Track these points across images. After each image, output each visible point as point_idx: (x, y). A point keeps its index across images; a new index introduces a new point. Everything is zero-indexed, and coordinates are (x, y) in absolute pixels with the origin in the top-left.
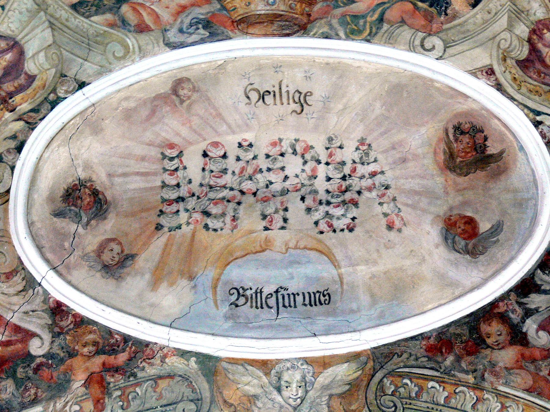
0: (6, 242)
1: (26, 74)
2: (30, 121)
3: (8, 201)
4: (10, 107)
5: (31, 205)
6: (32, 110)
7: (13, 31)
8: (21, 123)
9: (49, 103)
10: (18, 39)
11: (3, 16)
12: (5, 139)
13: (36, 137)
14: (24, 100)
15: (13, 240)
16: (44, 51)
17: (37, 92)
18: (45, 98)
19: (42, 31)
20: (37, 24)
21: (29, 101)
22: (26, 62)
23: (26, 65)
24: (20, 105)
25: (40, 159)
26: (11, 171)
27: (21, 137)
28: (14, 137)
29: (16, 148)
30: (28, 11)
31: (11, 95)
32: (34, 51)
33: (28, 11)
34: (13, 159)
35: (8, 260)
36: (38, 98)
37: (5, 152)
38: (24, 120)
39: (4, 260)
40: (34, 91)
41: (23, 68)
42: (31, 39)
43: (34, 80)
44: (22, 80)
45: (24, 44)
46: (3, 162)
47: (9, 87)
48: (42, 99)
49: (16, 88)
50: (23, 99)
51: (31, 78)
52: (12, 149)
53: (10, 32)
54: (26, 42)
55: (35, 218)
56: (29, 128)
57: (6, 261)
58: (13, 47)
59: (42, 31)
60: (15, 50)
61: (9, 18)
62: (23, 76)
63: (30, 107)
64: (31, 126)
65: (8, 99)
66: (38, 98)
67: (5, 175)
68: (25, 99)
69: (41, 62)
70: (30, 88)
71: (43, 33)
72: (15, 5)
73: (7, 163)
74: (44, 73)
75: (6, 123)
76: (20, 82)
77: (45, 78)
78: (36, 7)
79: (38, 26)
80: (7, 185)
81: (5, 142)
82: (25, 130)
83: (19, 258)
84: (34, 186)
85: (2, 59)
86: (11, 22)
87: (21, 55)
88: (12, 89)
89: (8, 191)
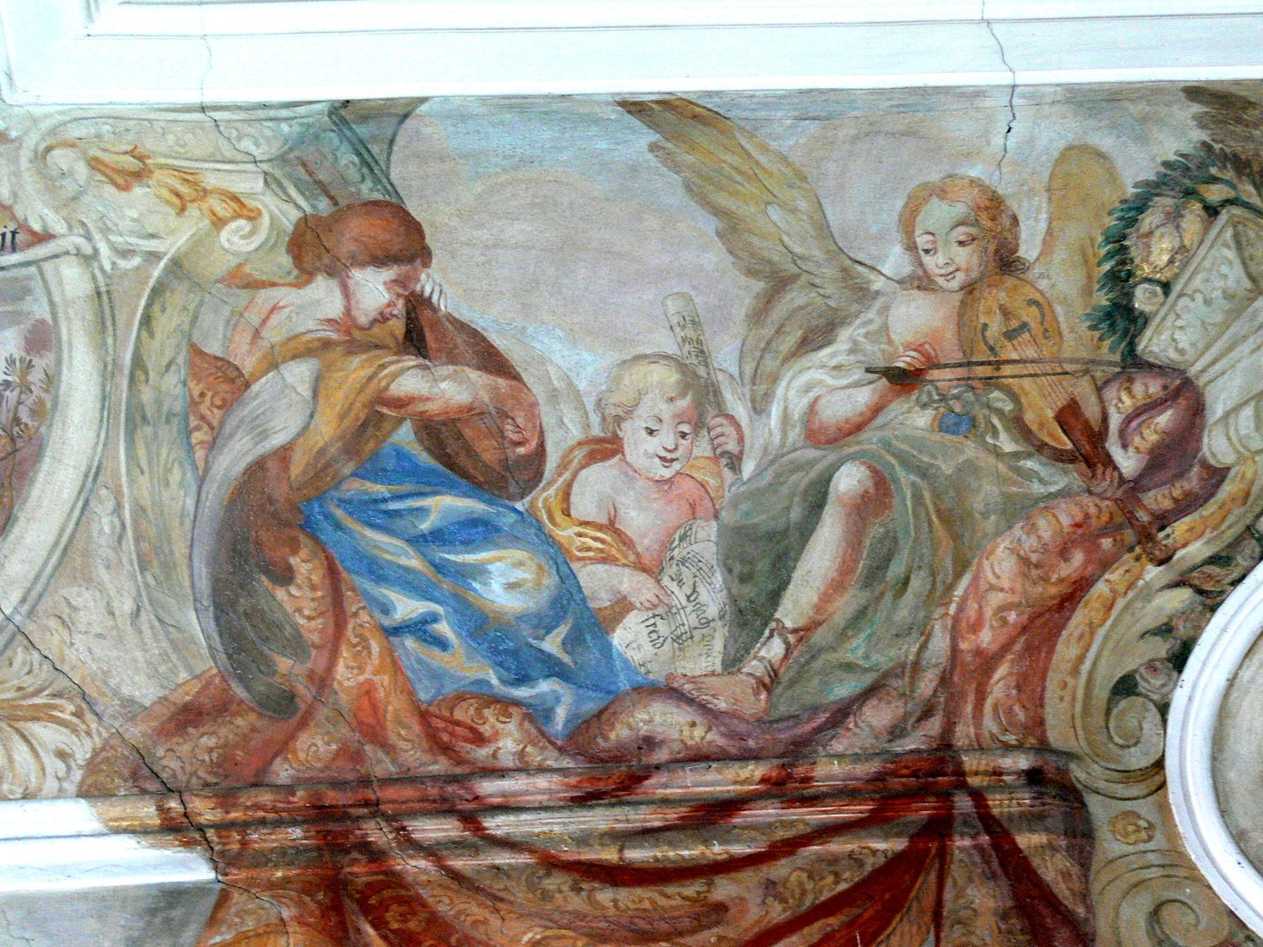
0: (1186, 878)
1: (1205, 465)
2: (1207, 587)
3: (1163, 785)
4: (1157, 553)
5: (1226, 796)
6: (1213, 560)
7: (1182, 352)
8: (1185, 594)
9: (1258, 540)
10: (1192, 371)
11: (1165, 309)
12: (1142, 636)
13: (1222, 625)
14: (1194, 534)
15: (1203, 872)
16: (1253, 403)
17: (1229, 511)
18: (1248, 528)
19: (1253, 351)
20: (1243, 333)
21: (1208, 535)
22: (1206, 432)
23: (1205, 440)
24: (1185, 545)
25: (1232, 682)
26: (1159, 717)
27: (1182, 630)
28: (1165, 630)
29: (1169, 660)
30: (1228, 296)
31: (1163, 520)
32: (1230, 405)
33: (1228, 296)
34: (1163, 685)
35: (1204, 921)
36: (1230, 527)
37: (1142, 670)
38: (1191, 586)
39: (1191, 918)
40: (1220, 508)
41: (1198, 449)
42: (1223, 373)
43: (1221, 481)
44: (1193, 480)
45: (1206, 385)
46: (1138, 695)
47: (1160, 498)
48: (1239, 528)
49: (1176, 501)
50: (1191, 529)
51: (1217, 475)
52: (1161, 660)
53: (1173, 355)
54: (1210, 382)
55: (1245, 823)
56: (1204, 605)
57: (1198, 922)
58: (1177, 393)
59: (1253, 351)
60: (1182, 402)
61: (1178, 316)
62: (1196, 469)
63: (1208, 552)
64: (1208, 602)
65: (1154, 531)
66: (1230, 527)
67: (1146, 726)
68: (1199, 529)
69: (1243, 432)
70: (1212, 501)
71: (1255, 356)
72: (1197, 282)
73: (1147, 697)
74: (1250, 462)
75: (1148, 594)
76: (1187, 486)
77: (1249, 475)
78: (1247, 284)
79: (1245, 338)
80: (1152, 751)
81: (1141, 642)
82: (1193, 611)
83: (1231, 914)
84: (1221, 751)
85: (1149, 427)
86: (1181, 328)
87: (1195, 415)
88: (1167, 504)
89: (1159, 764)
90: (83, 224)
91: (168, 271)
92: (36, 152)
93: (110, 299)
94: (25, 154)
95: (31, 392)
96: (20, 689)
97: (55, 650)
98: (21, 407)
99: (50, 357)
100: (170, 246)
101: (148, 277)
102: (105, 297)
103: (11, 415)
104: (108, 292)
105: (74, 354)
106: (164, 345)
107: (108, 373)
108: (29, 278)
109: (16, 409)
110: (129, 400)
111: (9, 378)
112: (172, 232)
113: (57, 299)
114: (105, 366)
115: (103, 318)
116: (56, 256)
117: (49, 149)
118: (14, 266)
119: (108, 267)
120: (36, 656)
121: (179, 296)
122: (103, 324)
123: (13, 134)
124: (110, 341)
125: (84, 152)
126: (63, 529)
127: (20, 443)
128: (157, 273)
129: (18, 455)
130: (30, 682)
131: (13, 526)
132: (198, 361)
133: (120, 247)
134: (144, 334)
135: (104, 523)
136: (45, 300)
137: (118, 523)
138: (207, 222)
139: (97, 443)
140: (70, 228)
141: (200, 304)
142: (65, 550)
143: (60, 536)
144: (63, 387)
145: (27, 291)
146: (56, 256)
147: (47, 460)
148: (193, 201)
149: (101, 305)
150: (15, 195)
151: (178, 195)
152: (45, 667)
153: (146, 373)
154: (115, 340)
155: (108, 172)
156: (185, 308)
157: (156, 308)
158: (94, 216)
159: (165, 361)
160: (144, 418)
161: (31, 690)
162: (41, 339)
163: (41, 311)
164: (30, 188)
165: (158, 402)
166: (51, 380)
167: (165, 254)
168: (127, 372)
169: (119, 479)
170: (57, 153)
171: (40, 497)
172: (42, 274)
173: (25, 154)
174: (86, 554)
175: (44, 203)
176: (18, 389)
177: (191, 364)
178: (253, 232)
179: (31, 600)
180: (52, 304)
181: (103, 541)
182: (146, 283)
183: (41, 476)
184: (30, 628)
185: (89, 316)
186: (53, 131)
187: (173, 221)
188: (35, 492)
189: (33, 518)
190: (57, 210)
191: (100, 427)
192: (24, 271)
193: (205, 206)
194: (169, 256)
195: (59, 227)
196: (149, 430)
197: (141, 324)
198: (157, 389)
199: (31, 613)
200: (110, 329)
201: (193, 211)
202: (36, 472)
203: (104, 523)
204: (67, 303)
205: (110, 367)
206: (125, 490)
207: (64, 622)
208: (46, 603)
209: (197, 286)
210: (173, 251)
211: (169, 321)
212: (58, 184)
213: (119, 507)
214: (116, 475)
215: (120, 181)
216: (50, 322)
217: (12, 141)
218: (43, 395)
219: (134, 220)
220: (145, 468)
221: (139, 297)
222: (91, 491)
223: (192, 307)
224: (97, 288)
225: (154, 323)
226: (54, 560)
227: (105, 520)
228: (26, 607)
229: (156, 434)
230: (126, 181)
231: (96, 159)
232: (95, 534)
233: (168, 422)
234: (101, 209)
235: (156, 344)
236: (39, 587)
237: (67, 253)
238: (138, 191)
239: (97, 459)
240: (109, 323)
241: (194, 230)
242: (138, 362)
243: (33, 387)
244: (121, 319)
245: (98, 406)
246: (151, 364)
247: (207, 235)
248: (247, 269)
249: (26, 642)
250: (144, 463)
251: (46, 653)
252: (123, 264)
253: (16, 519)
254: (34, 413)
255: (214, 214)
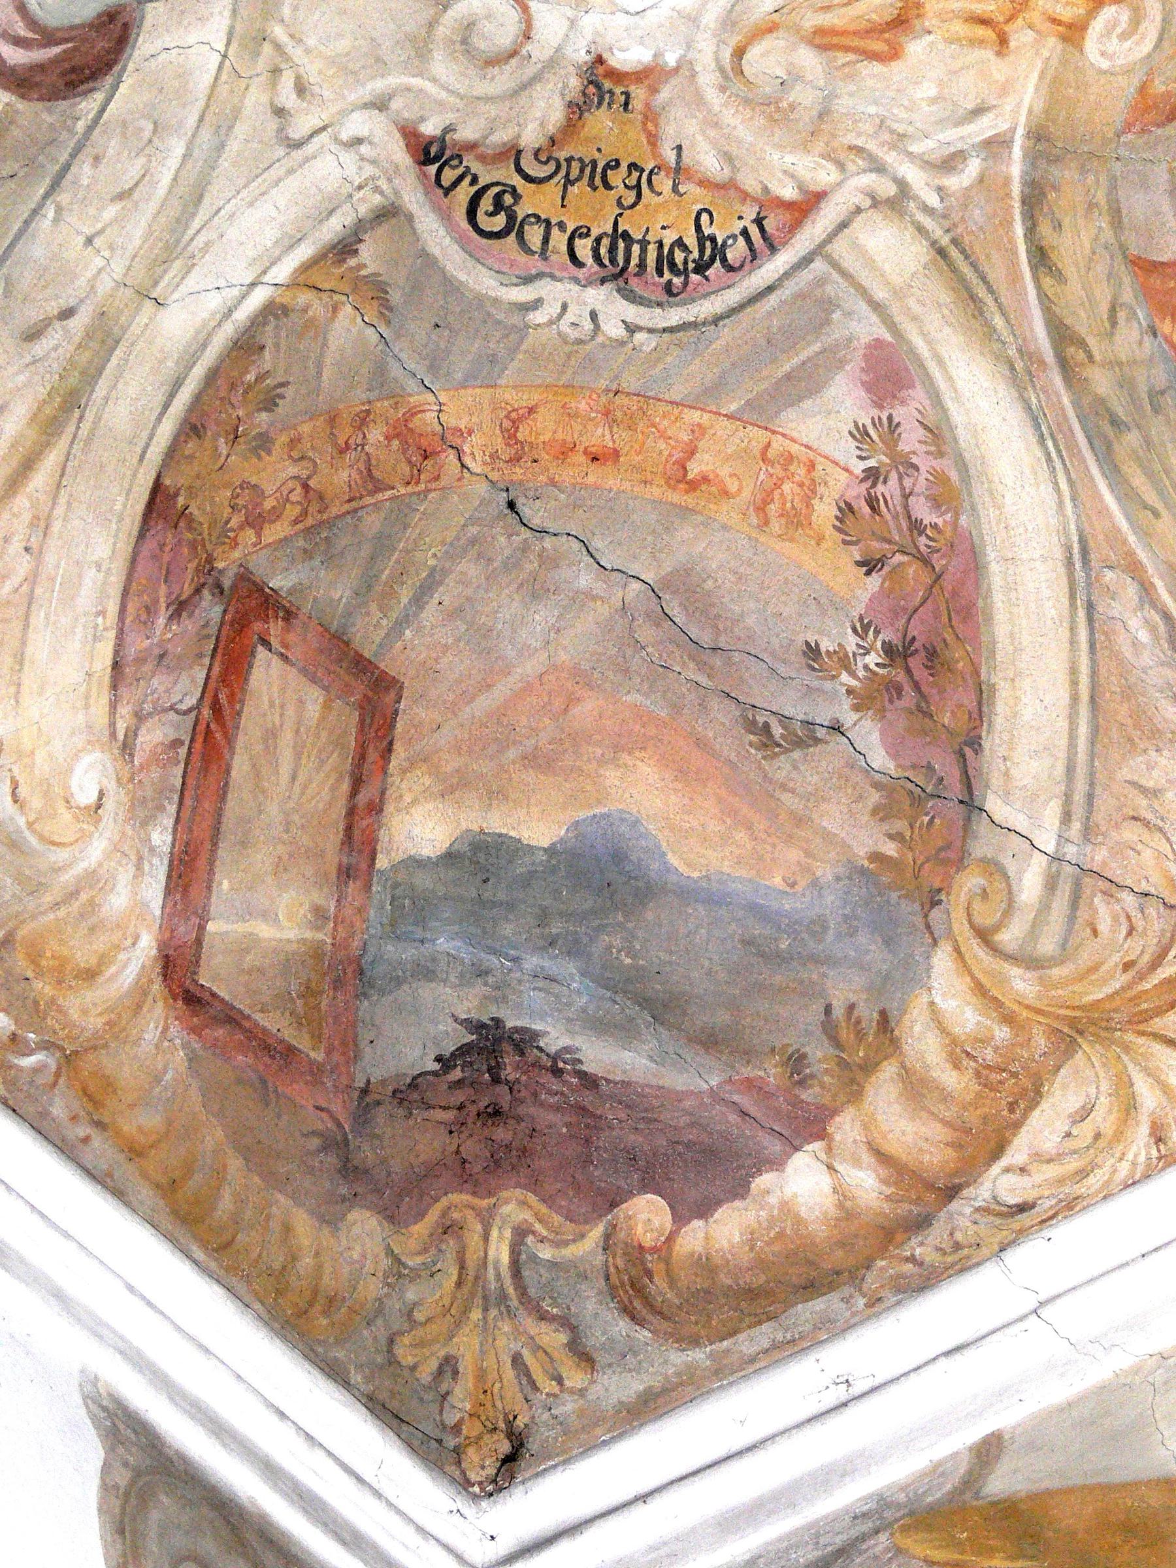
24: (148, 295)
90: (858, 150)
91: (1033, 158)
92: (722, 70)
93: (963, 252)
94: (707, 79)
95: (917, 468)
96: (1127, 966)
97: (1156, 878)
98: (912, 500)
99: (918, 396)
100: (1016, 112)
101: (1007, 181)
102: (954, 253)
103: (904, 525)
104: (955, 242)
105: (953, 372)
106: (1090, 281)
107: (1020, 373)
108: (821, 282)
109: (906, 507)
110: (1076, 405)
111: (872, 463)
112: (1004, 90)
113: (880, 294)
114: (1012, 368)
115: (968, 288)
116: (843, 225)
117: (739, 53)
118: (787, 275)
119: (933, 200)
120: (1129, 899)
121: (1072, 186)
122: (973, 297)
123: (671, 59)
124: (998, 321)
125: (797, 29)
126: (1073, 671)
127: (939, 563)
128: (1016, 168)
129: (947, 583)
130: (1141, 948)
131: (992, 704)
132: (1156, 281)
133: (934, 157)
134: (1047, 282)
135: (1136, 630)
136: (863, 306)
137: (1157, 618)
138: (1052, 41)
139: (1061, 504)
140: (841, 166)
141: (1113, 187)
142: (1093, 699)
143: (1074, 683)
144: (961, 433)
145: (829, 305)
146: (843, 225)
147: (994, 567)
148: (1011, 19)
149: (954, 270)
150: (728, 158)
151: (984, 22)
152: (1152, 912)
153: (1082, 344)
154: (1004, 314)
155: (856, 42)
156: (1091, 206)
157: (1045, 229)
158: (868, 127)
159: (1104, 308)
160: (1115, 422)
161: (1146, 958)
162: (890, 373)
163: (866, 328)
164: (744, 133)
165: (1126, 384)
166: (938, 435)
167: (1013, 130)
168: (1049, 356)
169: (1125, 542)
170: (753, 53)
171: (1012, 634)
172: (835, 265)
173: (707, 79)
174: (1128, 693)
175: (780, 147)
176: (894, 476)
177: (1147, 293)
178: (1137, 19)
179: (1078, 812)
180: (876, 306)
181: (1146, 659)
182: (1008, 195)
183: (998, 599)
184: (1099, 857)
185: (945, 297)
186: (729, 22)
187: (999, 69)
188: (1001, 629)
189: (1019, 674)
190: (805, 147)
191: (1053, 471)
192: (806, 276)
193: (1035, 16)
194: (1020, 132)
195: (824, 175)
196: (1132, 438)
197: (1034, 268)
198: (1113, 364)
199: (1088, 833)
200: (989, 300)
201: (1021, 37)
202: (989, 594)
203: (1136, 630)
204: (899, 293)
205: (1019, 365)
206: (1142, 555)
207: (1147, 824)
208: (1105, 804)
209: (1090, 160)
210: (1023, 120)
211: (1078, 240)
212: (784, 104)
213: (1146, 589)
214: (1114, 537)
215: (878, 46)
216: (888, 337)
217: (676, 70)
218: (937, 464)
219: (933, 101)
220: (1159, 506)
221: (1008, 223)
222: (1089, 585)
223: (1101, 196)
224: (934, 243)
225: (1053, 256)
226: (1083, 730)
227: (1134, 623)
228: (1076, 826)
229: (1148, 442)
230: (887, 41)
231: (820, 31)
232: (1127, 652)
233: (1157, 410)
234: (872, 110)
235: (1074, 286)
236: (1081, 787)
237: (858, 210)
238: (916, 48)
239: (1073, 527)
240: (981, 292)
241: (1039, 65)
242: (1062, 334)
243: (915, 460)
244: (997, 274)
245: (1033, 439)
246: (1081, 323)
247: (1064, 62)
248: (1159, 87)
249: (1101, 884)
250: (1151, 498)
251: (1144, 887)
252: (956, 182)
253: (993, 688)
254: (936, 503)
255: (1055, 21)
